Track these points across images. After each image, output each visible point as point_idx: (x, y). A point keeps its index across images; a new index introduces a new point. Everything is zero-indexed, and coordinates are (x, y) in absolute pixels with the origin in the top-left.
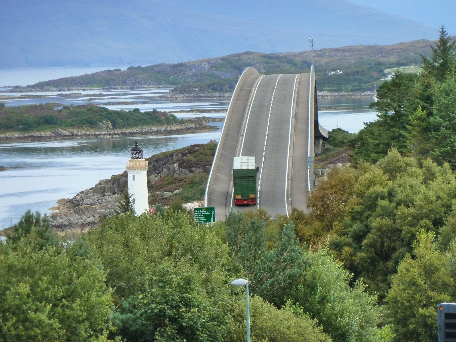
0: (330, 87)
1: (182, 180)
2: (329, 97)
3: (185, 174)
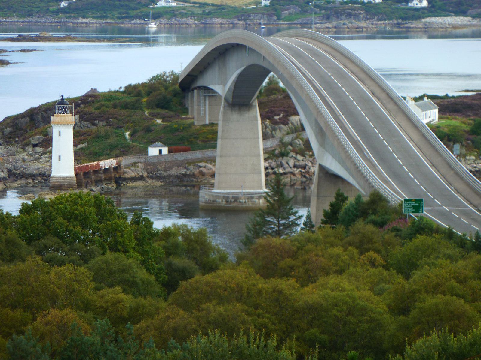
0: (94, 13)
1: (85, 134)
2: (95, 25)
3: (87, 127)
